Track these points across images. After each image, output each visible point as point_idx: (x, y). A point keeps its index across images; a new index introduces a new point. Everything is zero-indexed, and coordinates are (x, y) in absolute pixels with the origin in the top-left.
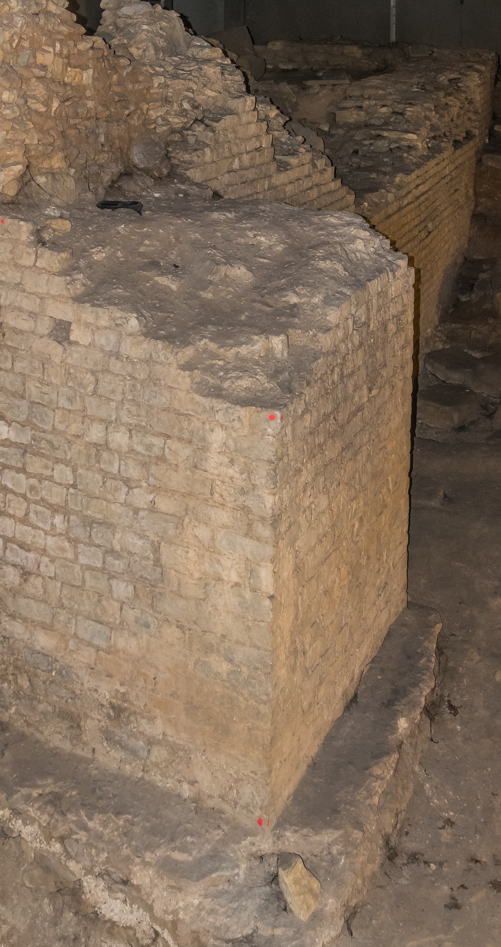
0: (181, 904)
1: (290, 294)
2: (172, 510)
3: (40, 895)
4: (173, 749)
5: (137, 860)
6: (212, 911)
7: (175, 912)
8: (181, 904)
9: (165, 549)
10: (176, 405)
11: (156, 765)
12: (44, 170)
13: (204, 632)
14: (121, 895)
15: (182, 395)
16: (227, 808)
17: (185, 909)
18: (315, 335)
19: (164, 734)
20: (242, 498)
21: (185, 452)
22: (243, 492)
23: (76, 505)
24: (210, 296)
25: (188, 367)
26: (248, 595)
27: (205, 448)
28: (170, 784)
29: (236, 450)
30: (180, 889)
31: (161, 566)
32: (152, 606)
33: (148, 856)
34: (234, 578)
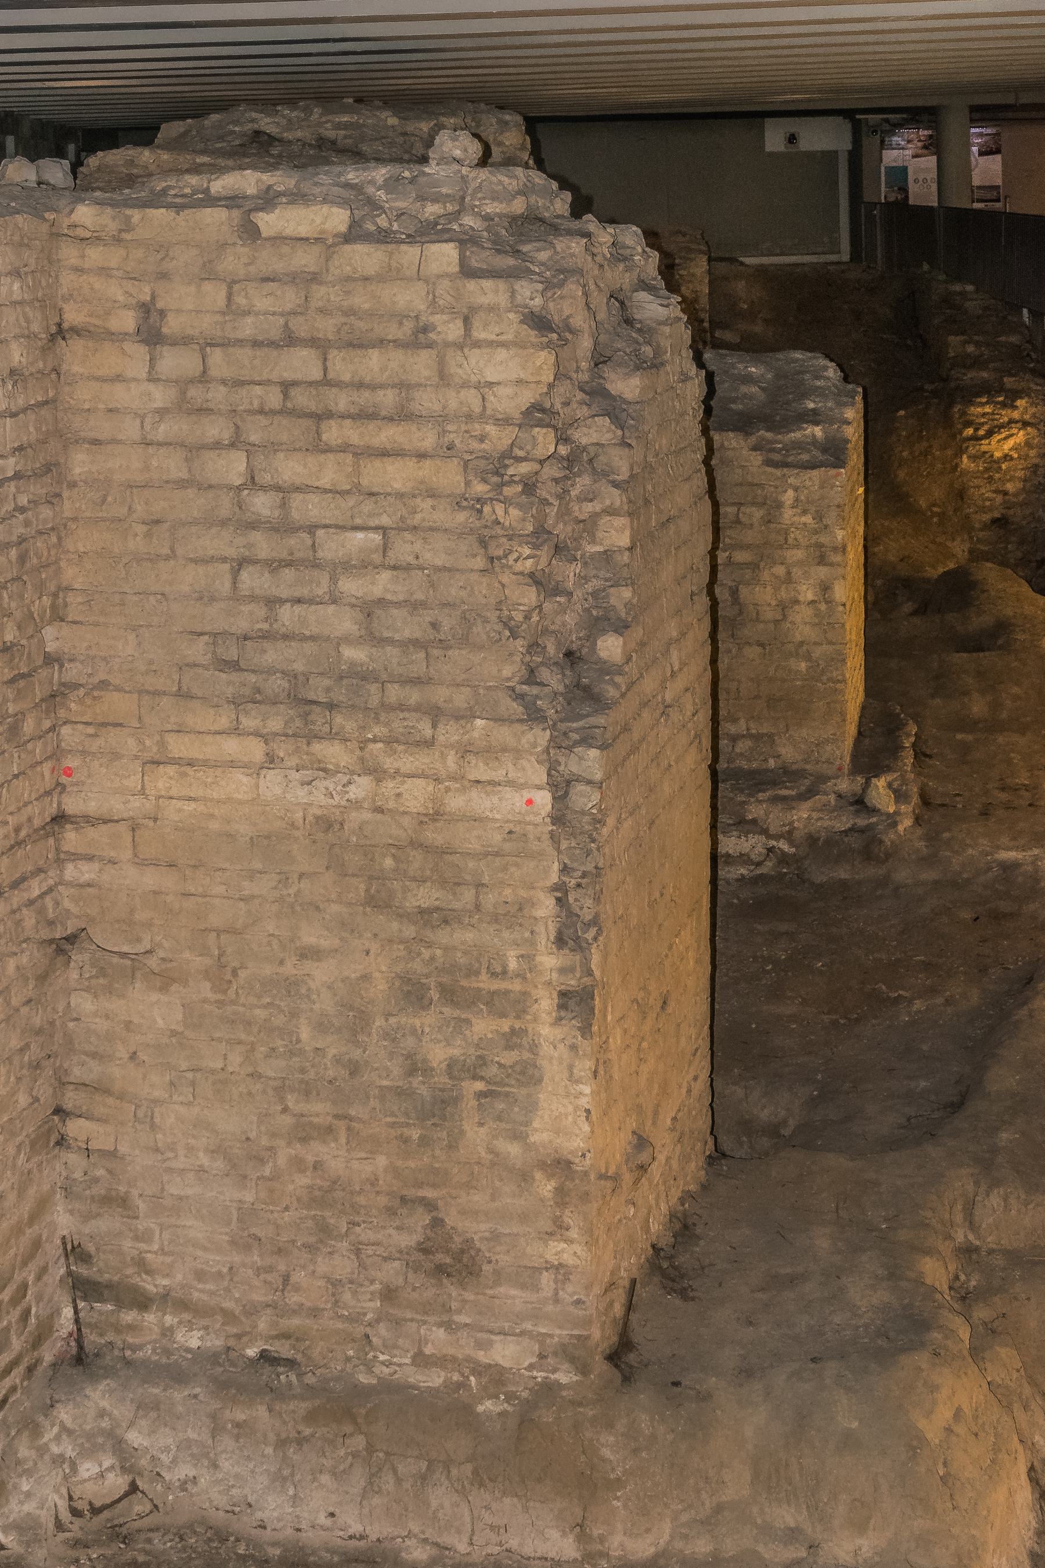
0: (795, 817)
1: (807, 402)
2: (749, 559)
3: (131, 1395)
4: (757, 738)
5: (752, 800)
6: (821, 819)
7: (791, 823)
8: (795, 817)
9: (744, 591)
10: (750, 479)
11: (742, 754)
12: (226, 442)
13: (783, 644)
14: (735, 833)
15: (754, 470)
16: (808, 767)
17: (798, 821)
18: (839, 427)
19: (748, 729)
20: (815, 537)
21: (758, 514)
22: (816, 532)
23: (333, 797)
24: (741, 407)
25: (755, 448)
26: (823, 607)
27: (779, 505)
28: (754, 765)
29: (808, 502)
30: (794, 808)
31: (739, 604)
32: (733, 635)
33: (761, 796)
34: (810, 596)
